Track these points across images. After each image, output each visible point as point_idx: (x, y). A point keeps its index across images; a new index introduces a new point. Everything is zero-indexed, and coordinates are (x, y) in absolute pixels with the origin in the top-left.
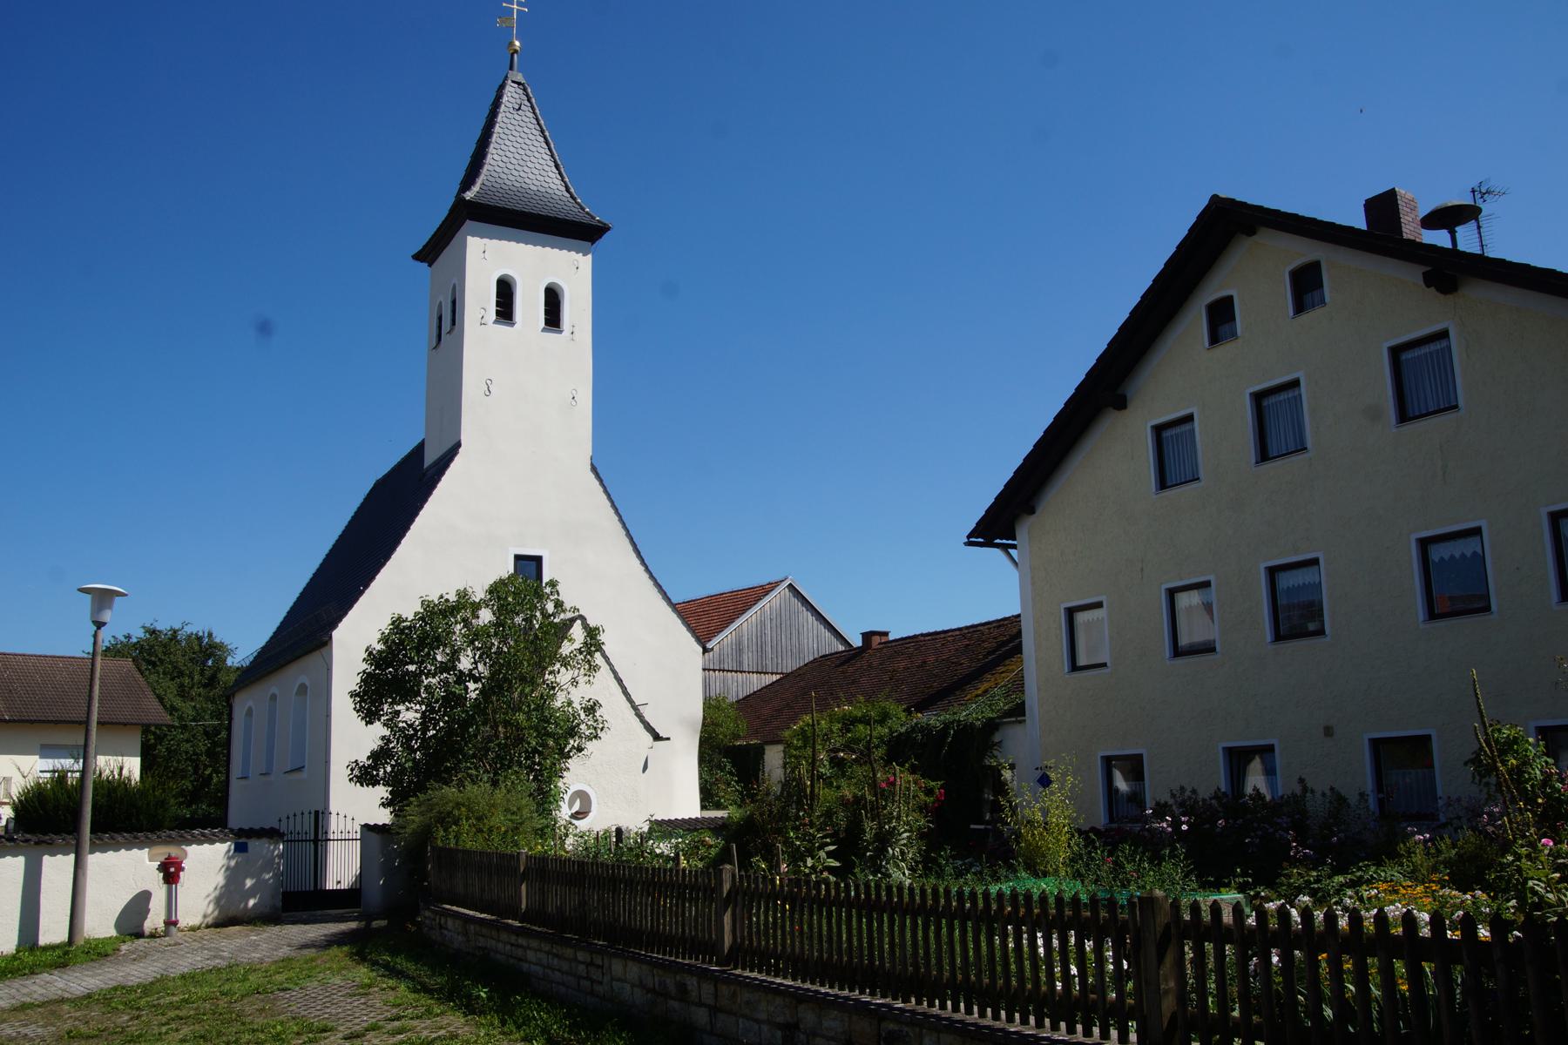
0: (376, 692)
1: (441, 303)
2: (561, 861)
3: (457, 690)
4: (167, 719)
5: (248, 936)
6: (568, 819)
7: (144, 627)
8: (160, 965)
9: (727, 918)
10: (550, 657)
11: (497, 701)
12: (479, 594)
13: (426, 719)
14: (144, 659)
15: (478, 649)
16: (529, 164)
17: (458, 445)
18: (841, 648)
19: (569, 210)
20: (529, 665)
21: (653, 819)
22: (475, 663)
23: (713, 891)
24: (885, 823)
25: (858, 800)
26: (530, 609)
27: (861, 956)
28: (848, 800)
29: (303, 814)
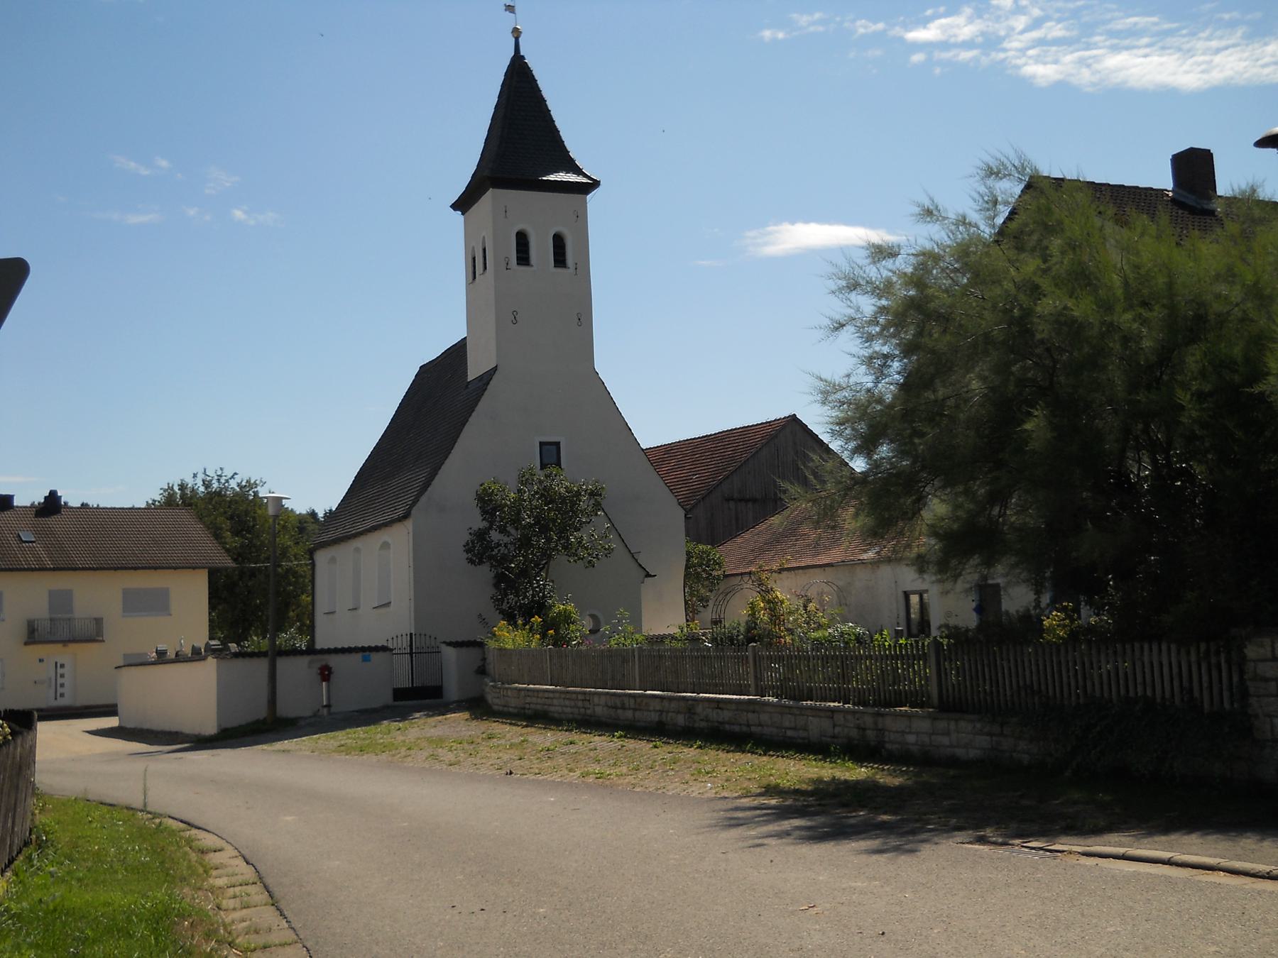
29: (397, 637)
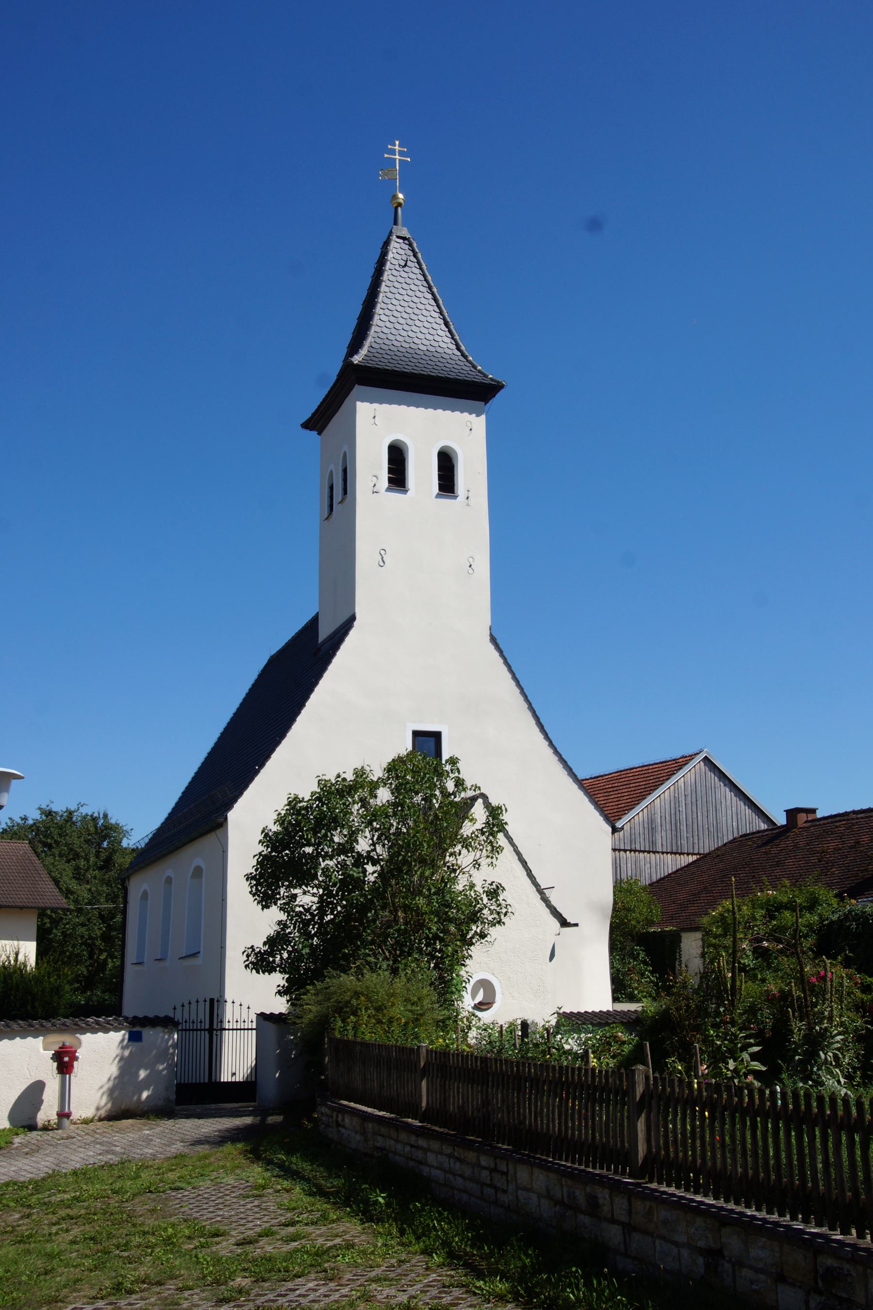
0: (273, 875)
1: (331, 472)
2: (462, 1056)
3: (355, 873)
4: (63, 902)
5: (140, 1130)
6: (471, 1010)
7: (40, 809)
8: (51, 1159)
9: (641, 1125)
10: (450, 838)
11: (397, 884)
12: (377, 773)
13: (324, 904)
14: (40, 842)
15: (377, 830)
16: (418, 323)
17: (353, 618)
18: (763, 826)
19: (457, 367)
20: (429, 847)
21: (561, 1011)
22: (374, 844)
23: (625, 1093)
24: (816, 1024)
25: (785, 996)
26: (429, 788)
27: (791, 1176)
28: (774, 995)
29: (197, 1002)
